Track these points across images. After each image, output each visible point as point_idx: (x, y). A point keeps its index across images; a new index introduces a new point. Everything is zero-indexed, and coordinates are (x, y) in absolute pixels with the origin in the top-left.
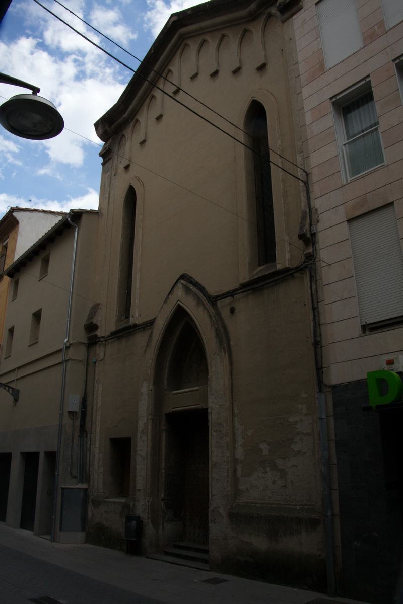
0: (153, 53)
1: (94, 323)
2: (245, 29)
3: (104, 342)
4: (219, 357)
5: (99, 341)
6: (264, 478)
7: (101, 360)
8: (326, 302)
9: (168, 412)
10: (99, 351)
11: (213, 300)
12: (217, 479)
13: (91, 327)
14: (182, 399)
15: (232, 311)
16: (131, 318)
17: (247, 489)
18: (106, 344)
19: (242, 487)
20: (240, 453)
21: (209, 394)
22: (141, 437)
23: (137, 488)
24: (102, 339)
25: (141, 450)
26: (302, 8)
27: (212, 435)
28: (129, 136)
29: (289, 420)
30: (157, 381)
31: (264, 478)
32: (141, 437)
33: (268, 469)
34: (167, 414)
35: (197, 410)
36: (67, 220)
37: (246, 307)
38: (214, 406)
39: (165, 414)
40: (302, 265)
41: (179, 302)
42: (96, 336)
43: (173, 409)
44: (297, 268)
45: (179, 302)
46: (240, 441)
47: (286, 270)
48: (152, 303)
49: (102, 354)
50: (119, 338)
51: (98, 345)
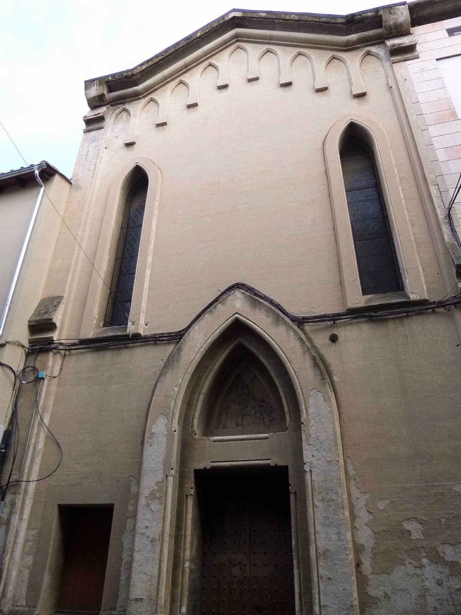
0: (199, 38)
1: (54, 321)
2: (333, 55)
3: (63, 352)
4: (322, 394)
5: (55, 348)
6: (418, 576)
7: (55, 377)
9: (202, 468)
10: (52, 363)
11: (300, 322)
12: (329, 579)
13: (41, 326)
14: (240, 448)
15: (334, 339)
16: (130, 323)
17: (386, 594)
18: (65, 355)
19: (373, 592)
20: (365, 537)
21: (304, 444)
22: (148, 505)
23: (133, 596)
24: (61, 347)
25: (147, 527)
26: (103, 128)
27: (314, 506)
28: (109, 116)
29: (455, 488)
30: (186, 421)
31: (418, 576)
32: (148, 505)
33: (425, 561)
34: (200, 470)
35: (276, 467)
36: (34, 171)
37: (356, 338)
38: (315, 463)
39: (196, 471)
40: (447, 300)
41: (236, 315)
42: (50, 341)
43: (212, 464)
44: (440, 302)
45: (236, 315)
46: (364, 517)
47: (422, 303)
49: (57, 368)
50: (98, 350)
51: (51, 354)
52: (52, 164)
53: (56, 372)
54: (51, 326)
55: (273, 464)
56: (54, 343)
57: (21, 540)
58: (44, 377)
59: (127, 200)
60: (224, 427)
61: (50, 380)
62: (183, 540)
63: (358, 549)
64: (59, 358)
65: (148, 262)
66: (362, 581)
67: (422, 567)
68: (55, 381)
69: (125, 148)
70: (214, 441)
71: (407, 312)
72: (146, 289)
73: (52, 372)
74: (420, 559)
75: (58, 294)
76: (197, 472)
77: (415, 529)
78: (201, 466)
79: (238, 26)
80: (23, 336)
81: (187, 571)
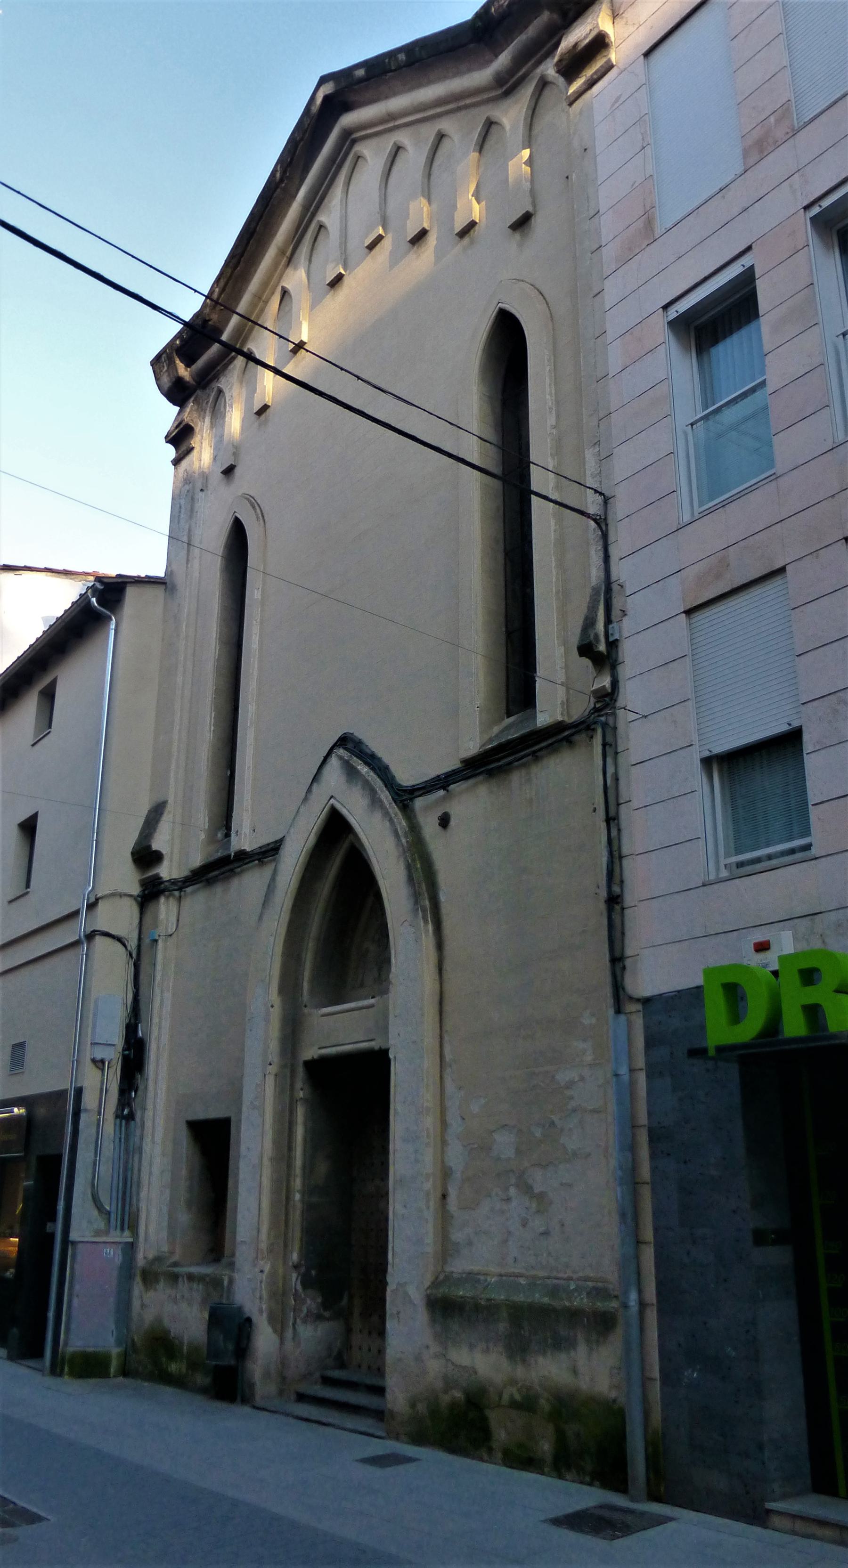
7: (171, 935)
8: (635, 804)
14: (337, 1030)
33: (512, 1191)
42: (157, 879)
48: (278, 811)
50: (210, 883)
51: (162, 900)
52: (111, 570)
53: (172, 929)
54: (157, 858)
55: (377, 1048)
56: (163, 882)
57: (156, 1170)
58: (157, 938)
59: (504, 391)
60: (362, 985)
61: (165, 941)
62: (794, 1046)
63: (446, 1173)
64: (173, 903)
65: (250, 715)
66: (445, 1219)
67: (508, 1200)
68: (171, 941)
69: (517, 236)
70: (323, 1015)
71: (534, 752)
72: (249, 768)
73: (167, 929)
74: (507, 1189)
75: (162, 799)
76: (310, 1065)
77: (505, 1143)
78: (306, 1059)
79: (341, 93)
80: (126, 878)
81: (299, 1206)
